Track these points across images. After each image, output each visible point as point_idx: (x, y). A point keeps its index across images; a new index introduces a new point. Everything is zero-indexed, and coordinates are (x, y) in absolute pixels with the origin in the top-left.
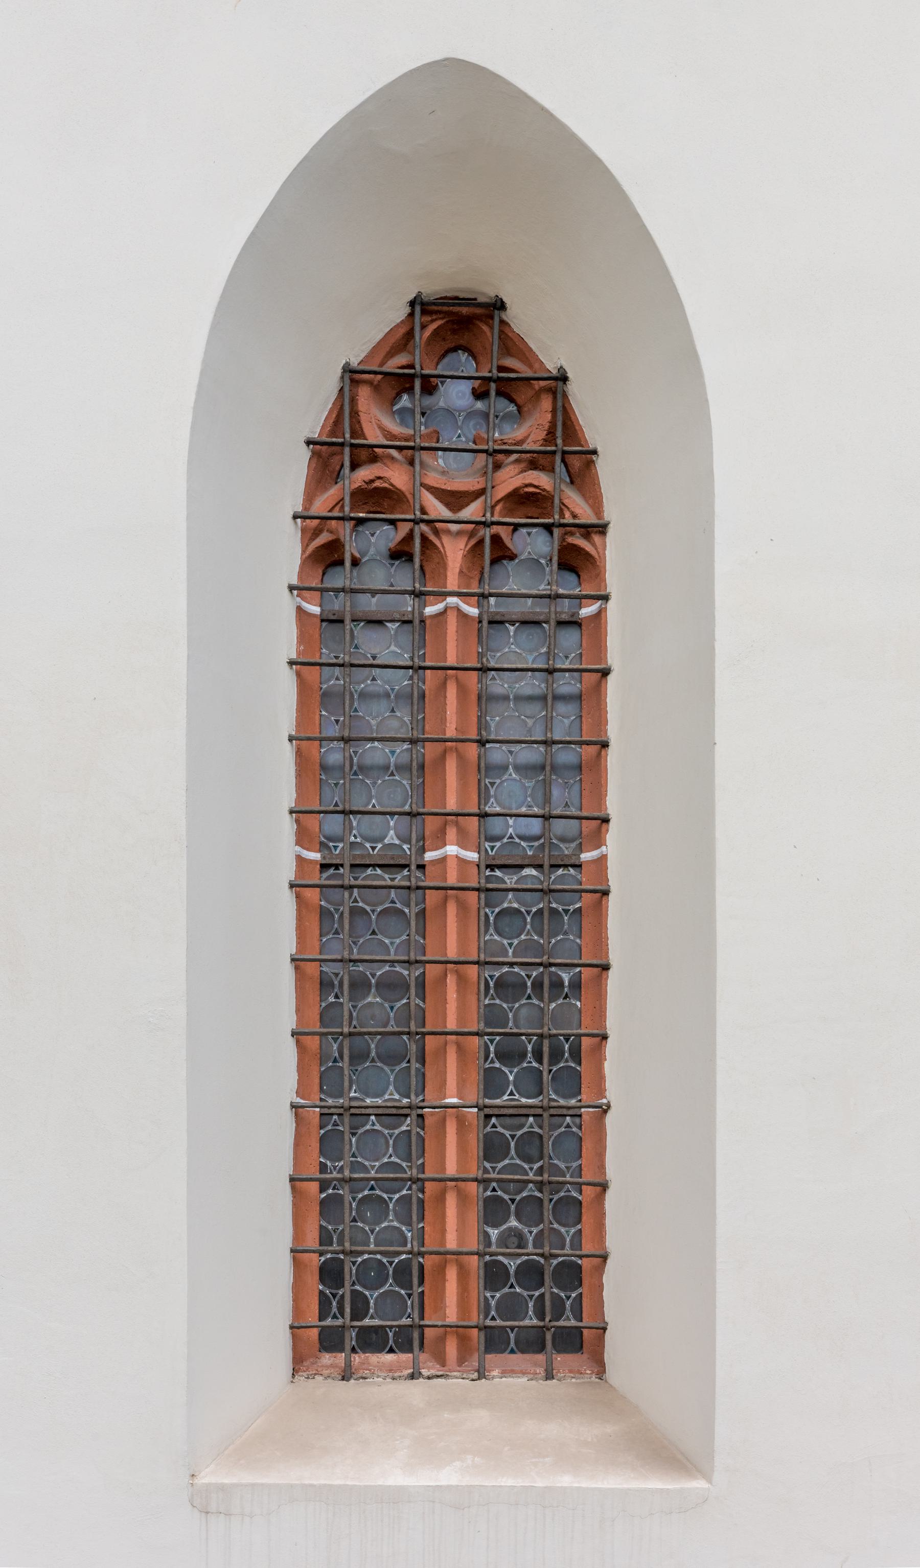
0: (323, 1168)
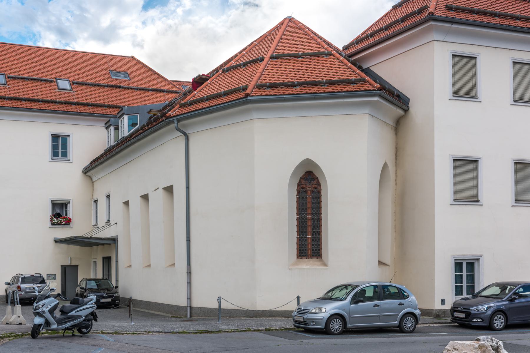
0: (299, 242)
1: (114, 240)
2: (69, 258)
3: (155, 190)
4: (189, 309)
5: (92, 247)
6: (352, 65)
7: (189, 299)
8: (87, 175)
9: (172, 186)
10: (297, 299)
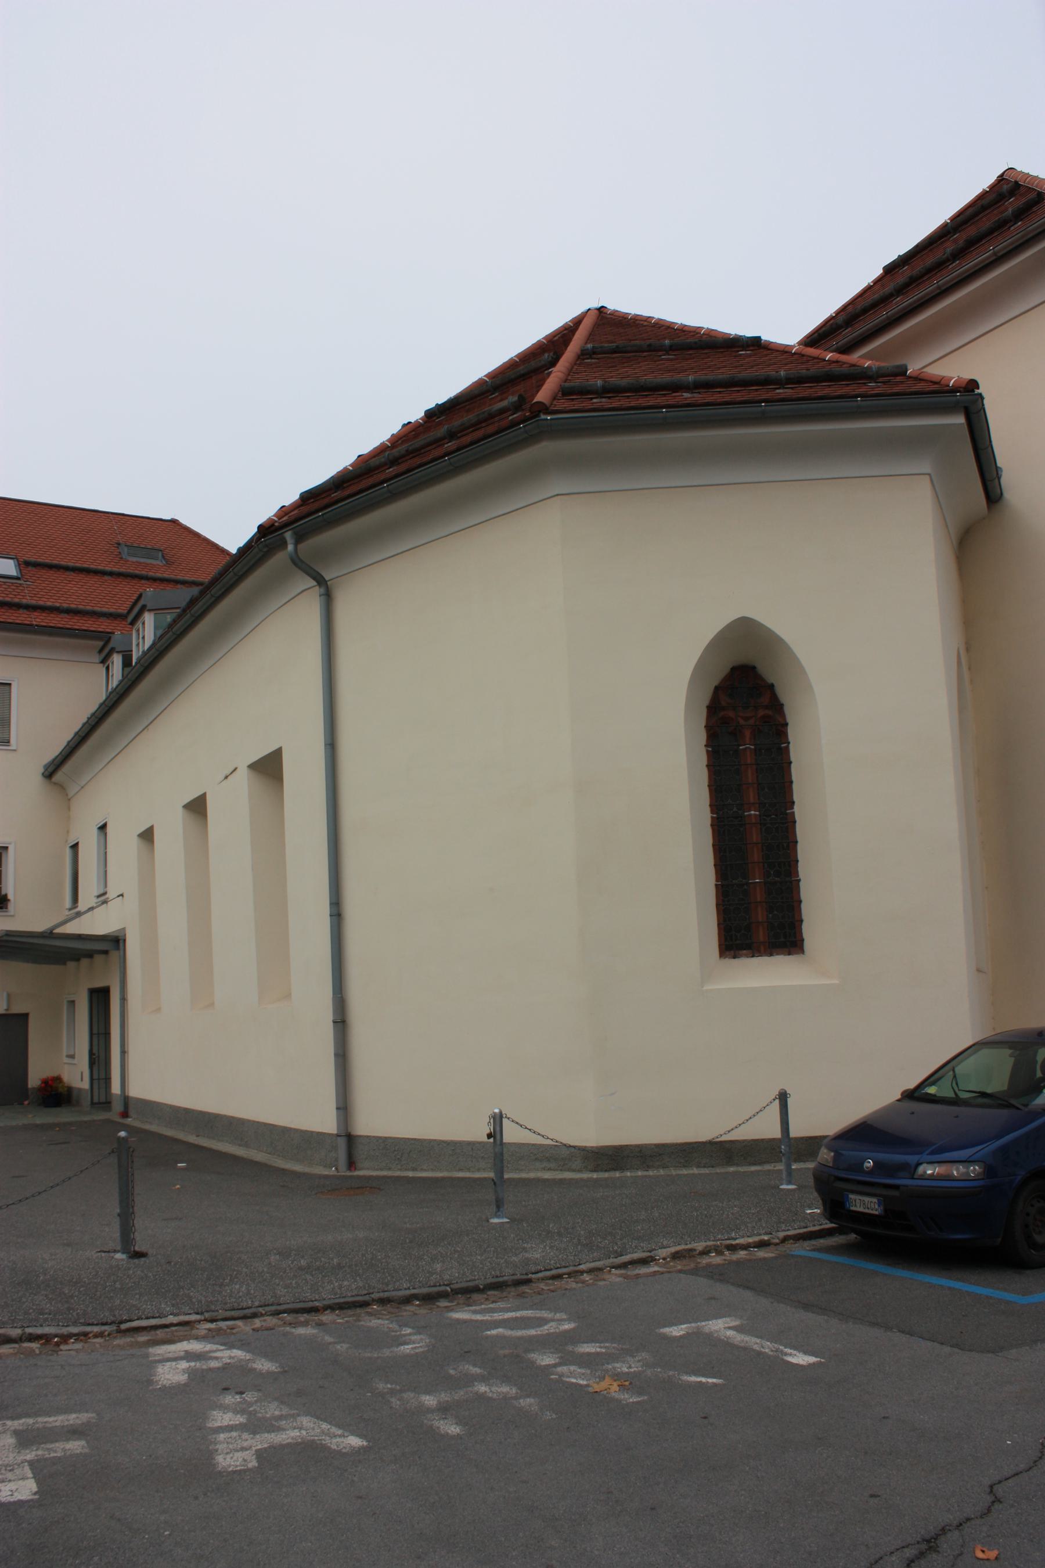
1: (116, 942)
2: (5, 994)
3: (226, 777)
4: (342, 1143)
5: (65, 964)
6: (839, 355)
7: (344, 1107)
8: (55, 784)
9: (277, 755)
10: (777, 1101)
